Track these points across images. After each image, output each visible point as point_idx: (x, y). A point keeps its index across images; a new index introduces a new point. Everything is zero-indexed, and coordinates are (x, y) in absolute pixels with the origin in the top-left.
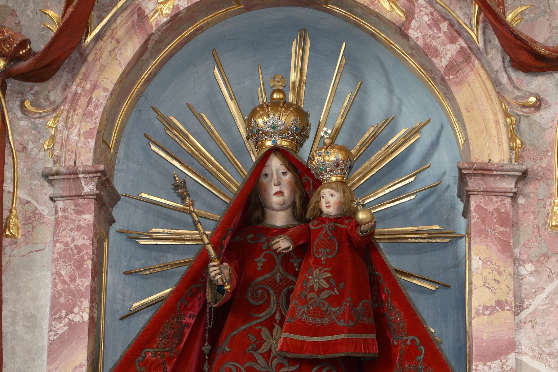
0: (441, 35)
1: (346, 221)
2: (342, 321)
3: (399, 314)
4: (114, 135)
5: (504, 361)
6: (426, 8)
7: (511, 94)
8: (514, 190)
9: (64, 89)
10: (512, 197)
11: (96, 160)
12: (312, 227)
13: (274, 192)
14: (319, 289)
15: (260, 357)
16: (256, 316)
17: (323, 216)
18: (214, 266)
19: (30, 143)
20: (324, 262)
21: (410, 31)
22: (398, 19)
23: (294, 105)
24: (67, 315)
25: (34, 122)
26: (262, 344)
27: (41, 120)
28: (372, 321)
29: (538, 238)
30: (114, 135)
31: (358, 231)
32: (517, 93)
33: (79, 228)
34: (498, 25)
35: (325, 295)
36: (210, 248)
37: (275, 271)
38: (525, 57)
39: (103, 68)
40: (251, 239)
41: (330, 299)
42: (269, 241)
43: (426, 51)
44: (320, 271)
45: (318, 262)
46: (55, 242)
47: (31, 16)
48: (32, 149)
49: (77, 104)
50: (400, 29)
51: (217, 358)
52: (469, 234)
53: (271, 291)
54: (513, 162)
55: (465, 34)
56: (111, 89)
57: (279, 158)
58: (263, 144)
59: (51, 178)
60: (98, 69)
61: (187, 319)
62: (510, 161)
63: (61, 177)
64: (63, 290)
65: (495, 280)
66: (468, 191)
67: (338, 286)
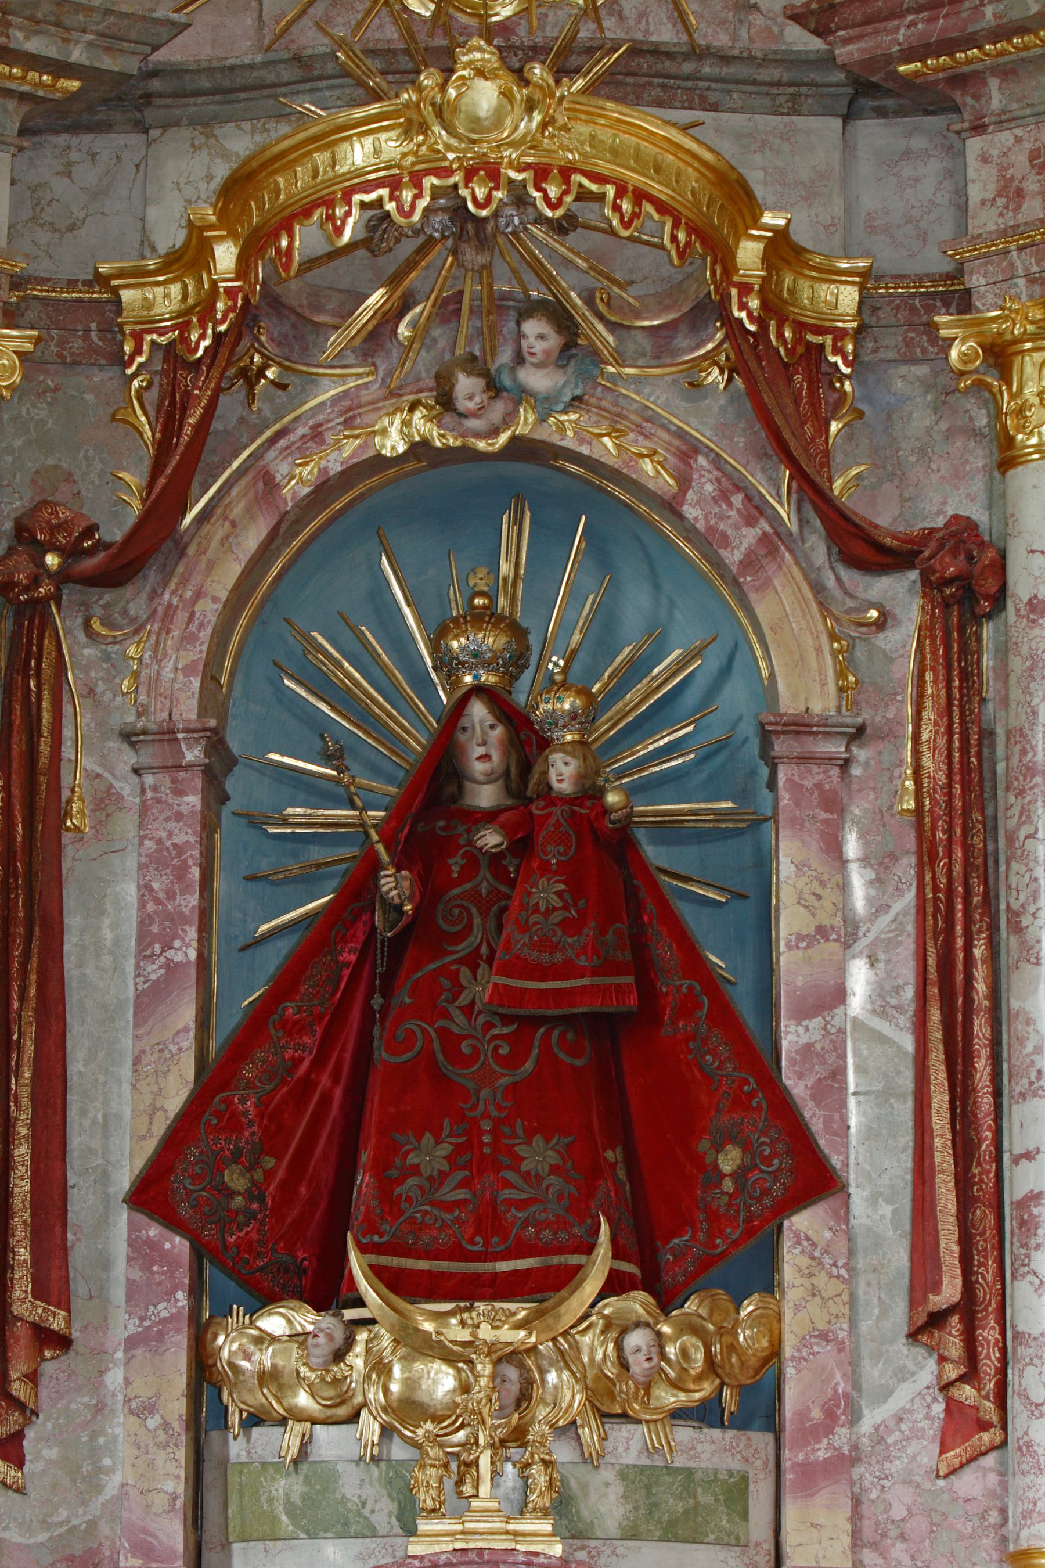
0: (733, 513)
1: (589, 803)
2: (583, 958)
3: (670, 946)
4: (228, 665)
5: (828, 1019)
6: (709, 472)
7: (842, 604)
8: (844, 756)
9: (151, 598)
10: (841, 766)
11: (203, 712)
12: (536, 812)
13: (476, 755)
14: (547, 909)
15: (458, 1012)
16: (451, 948)
17: (553, 794)
18: (387, 876)
19: (100, 683)
20: (555, 867)
21: (685, 508)
22: (667, 488)
23: (506, 618)
24: (163, 951)
25: (106, 651)
26: (460, 992)
27: (117, 647)
28: (628, 956)
29: (881, 828)
30: (228, 665)
31: (607, 821)
32: (850, 603)
33: (179, 817)
34: (819, 502)
35: (557, 917)
36: (380, 848)
37: (479, 878)
38: (860, 549)
39: (211, 566)
40: (441, 829)
41: (566, 925)
42: (469, 831)
43: (710, 538)
44: (549, 880)
45: (545, 868)
46: (142, 838)
47: (97, 483)
48: (104, 693)
49: (171, 622)
50: (670, 504)
51: (393, 1013)
52: (774, 817)
53: (474, 910)
54: (844, 709)
55: (770, 512)
56: (224, 599)
57: (484, 703)
58: (459, 680)
59: (134, 739)
60: (203, 567)
61: (345, 955)
62: (839, 709)
63: (150, 738)
64: (156, 913)
65: (814, 894)
66: (774, 758)
67: (576, 905)
